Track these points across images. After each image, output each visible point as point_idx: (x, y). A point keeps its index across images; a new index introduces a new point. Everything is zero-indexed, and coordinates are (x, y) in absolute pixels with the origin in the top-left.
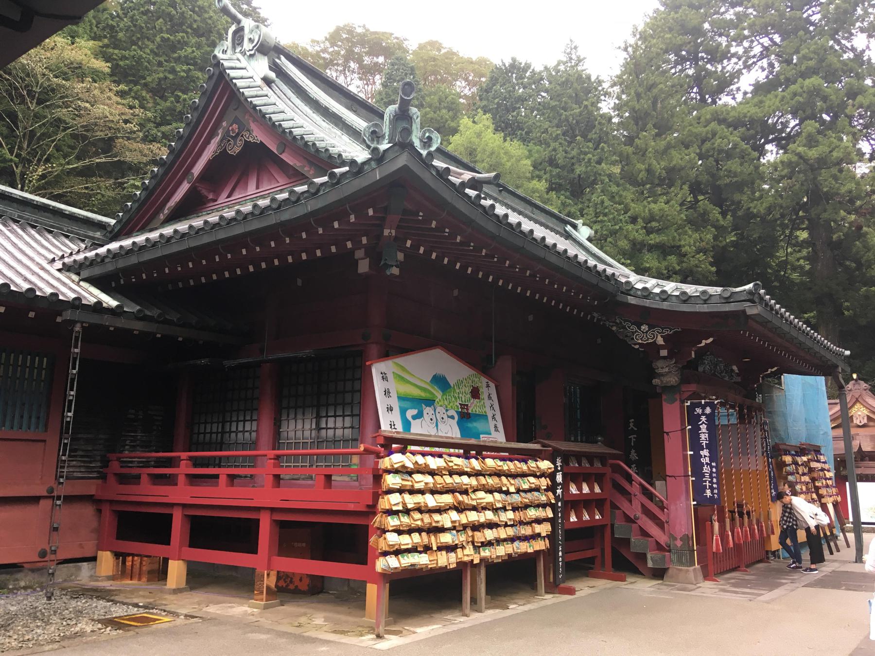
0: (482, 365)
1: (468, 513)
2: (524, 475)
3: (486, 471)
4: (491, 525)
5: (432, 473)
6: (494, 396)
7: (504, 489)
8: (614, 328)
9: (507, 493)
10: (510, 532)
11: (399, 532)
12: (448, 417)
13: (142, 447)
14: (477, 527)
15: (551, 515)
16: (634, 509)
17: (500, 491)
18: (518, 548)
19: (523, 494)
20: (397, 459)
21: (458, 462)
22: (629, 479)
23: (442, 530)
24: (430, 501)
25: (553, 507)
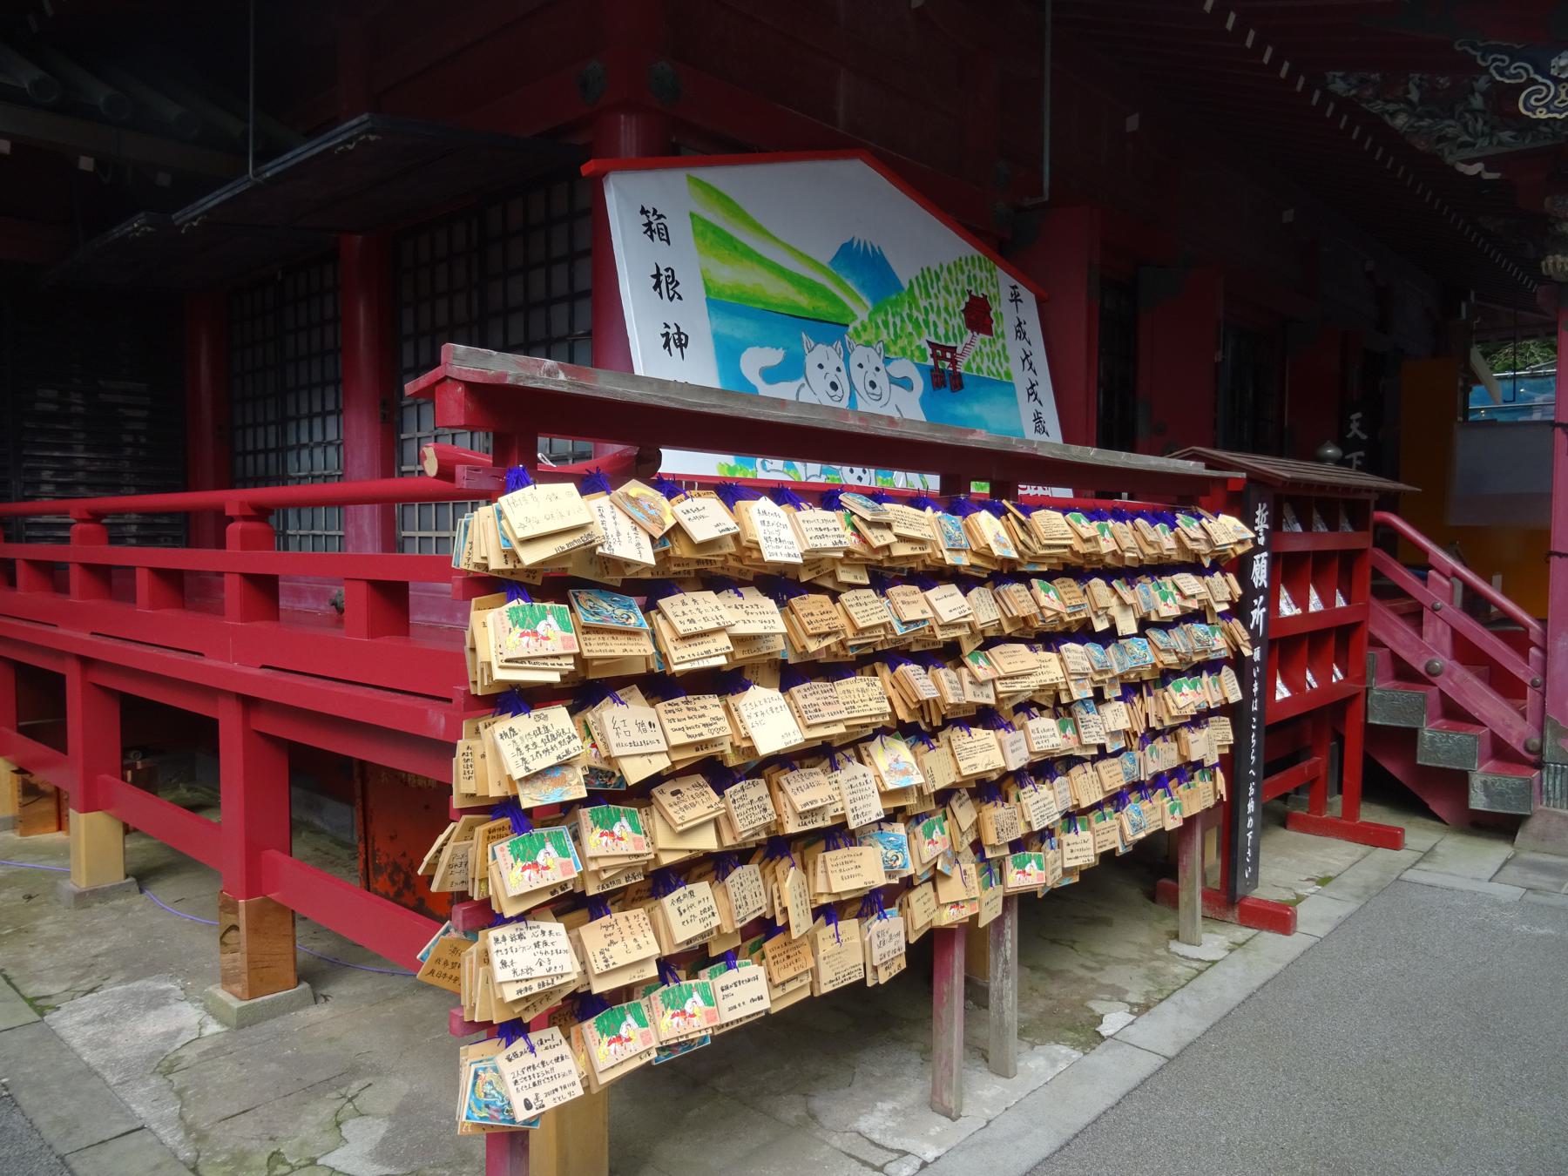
0: (1002, 241)
1: (959, 737)
2: (1160, 568)
3: (1037, 559)
4: (1045, 769)
5: (781, 584)
6: (1034, 329)
7: (1100, 626)
8: (1401, 121)
9: (1110, 637)
10: (1114, 775)
11: (572, 905)
12: (893, 381)
13: (92, 486)
14: (989, 789)
15: (1235, 695)
16: (1431, 649)
17: (1083, 633)
18: (1137, 827)
19: (1155, 635)
20: (539, 514)
21: (924, 529)
22: (1422, 566)
23: (838, 835)
24: (769, 720)
25: (1238, 662)
